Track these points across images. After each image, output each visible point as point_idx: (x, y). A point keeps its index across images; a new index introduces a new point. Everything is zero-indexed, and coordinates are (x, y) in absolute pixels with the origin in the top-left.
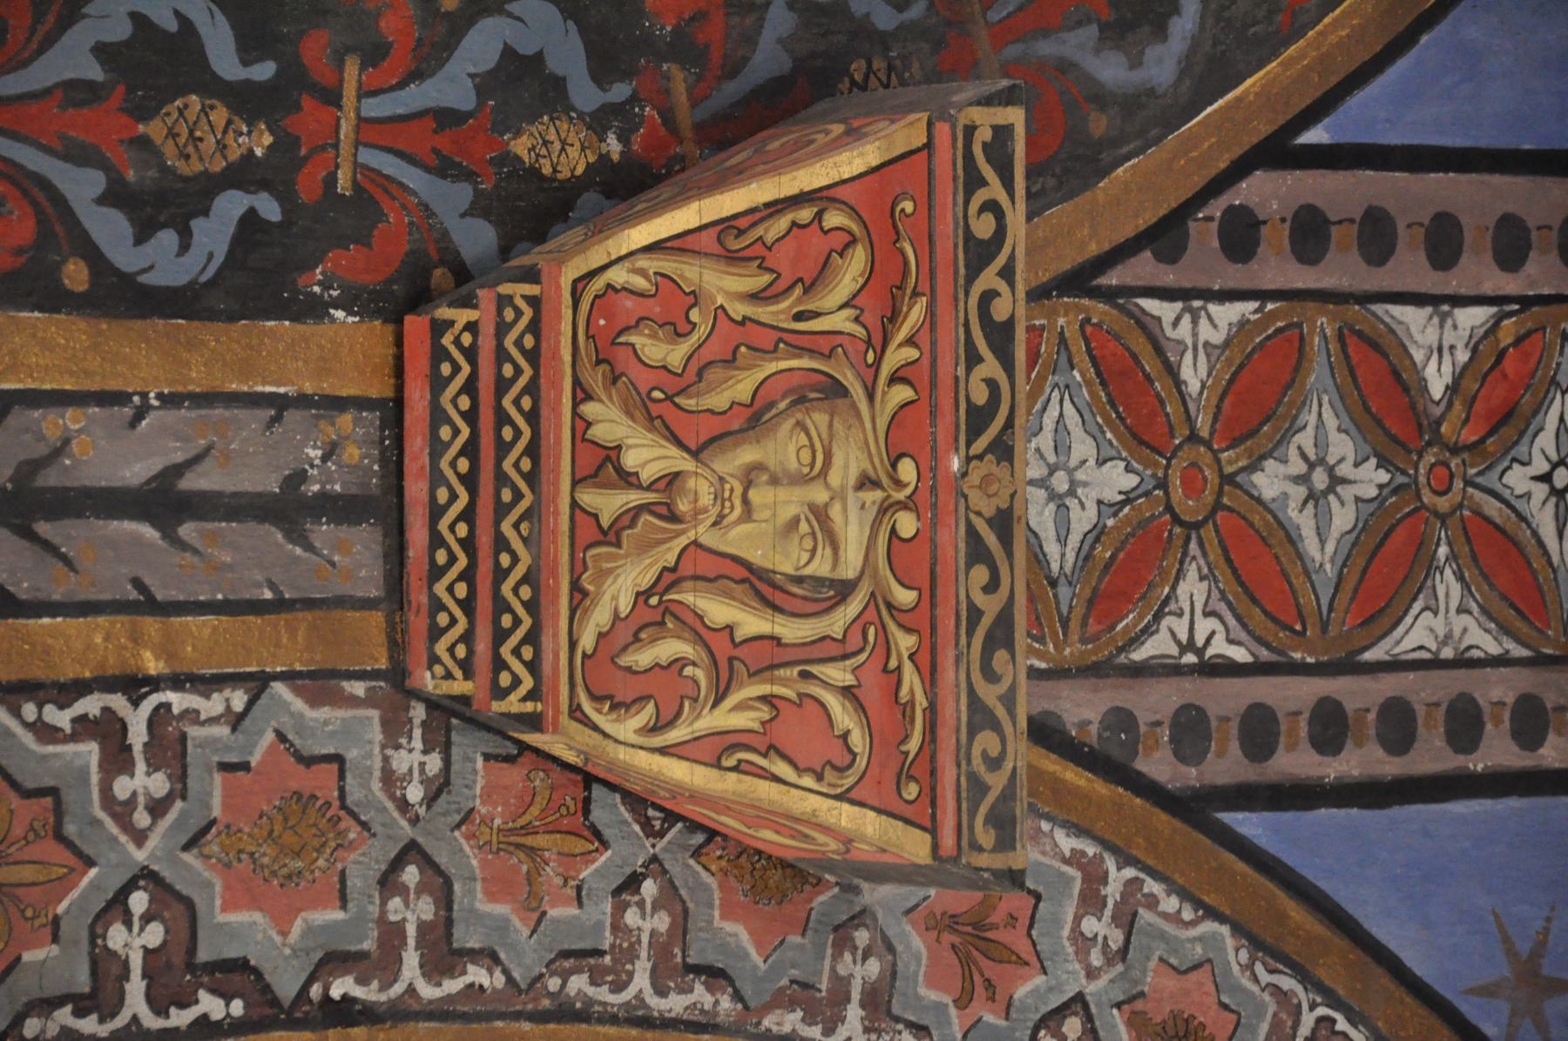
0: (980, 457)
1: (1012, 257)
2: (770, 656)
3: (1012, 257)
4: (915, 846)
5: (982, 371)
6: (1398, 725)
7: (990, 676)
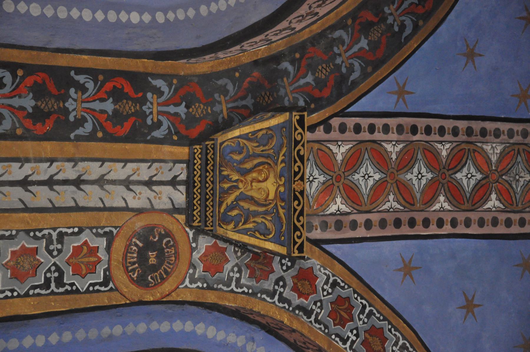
0: (297, 181)
1: (304, 143)
2: (256, 214)
3: (304, 143)
4: (283, 250)
5: (297, 164)
6: (440, 223)
7: (299, 221)
